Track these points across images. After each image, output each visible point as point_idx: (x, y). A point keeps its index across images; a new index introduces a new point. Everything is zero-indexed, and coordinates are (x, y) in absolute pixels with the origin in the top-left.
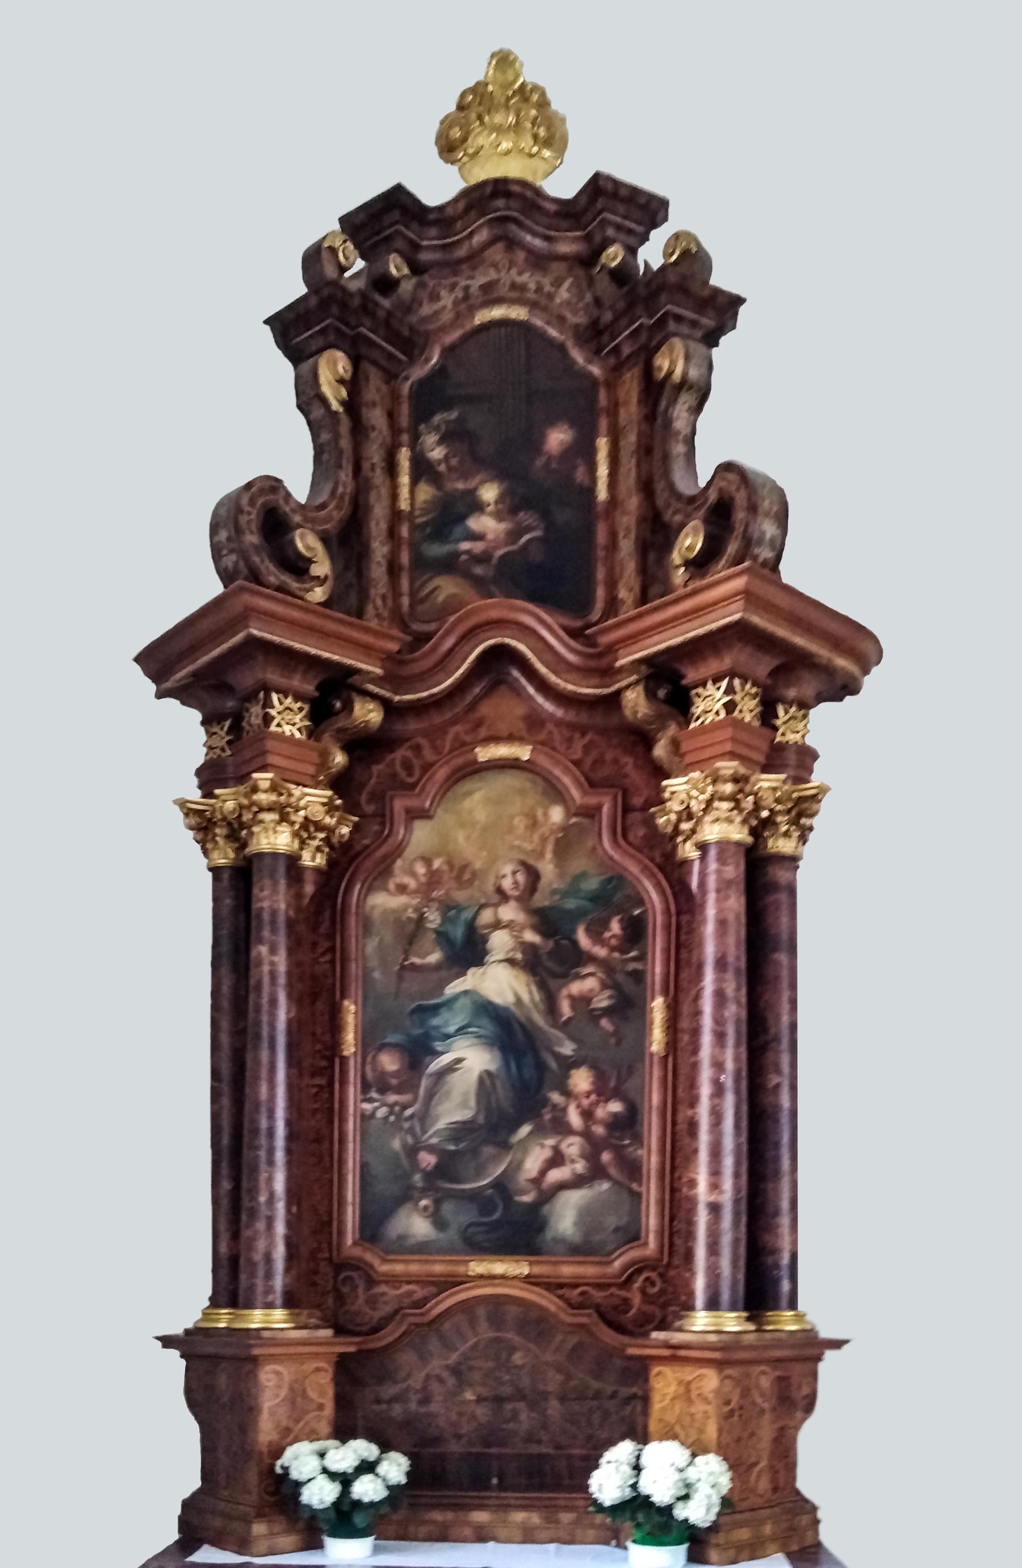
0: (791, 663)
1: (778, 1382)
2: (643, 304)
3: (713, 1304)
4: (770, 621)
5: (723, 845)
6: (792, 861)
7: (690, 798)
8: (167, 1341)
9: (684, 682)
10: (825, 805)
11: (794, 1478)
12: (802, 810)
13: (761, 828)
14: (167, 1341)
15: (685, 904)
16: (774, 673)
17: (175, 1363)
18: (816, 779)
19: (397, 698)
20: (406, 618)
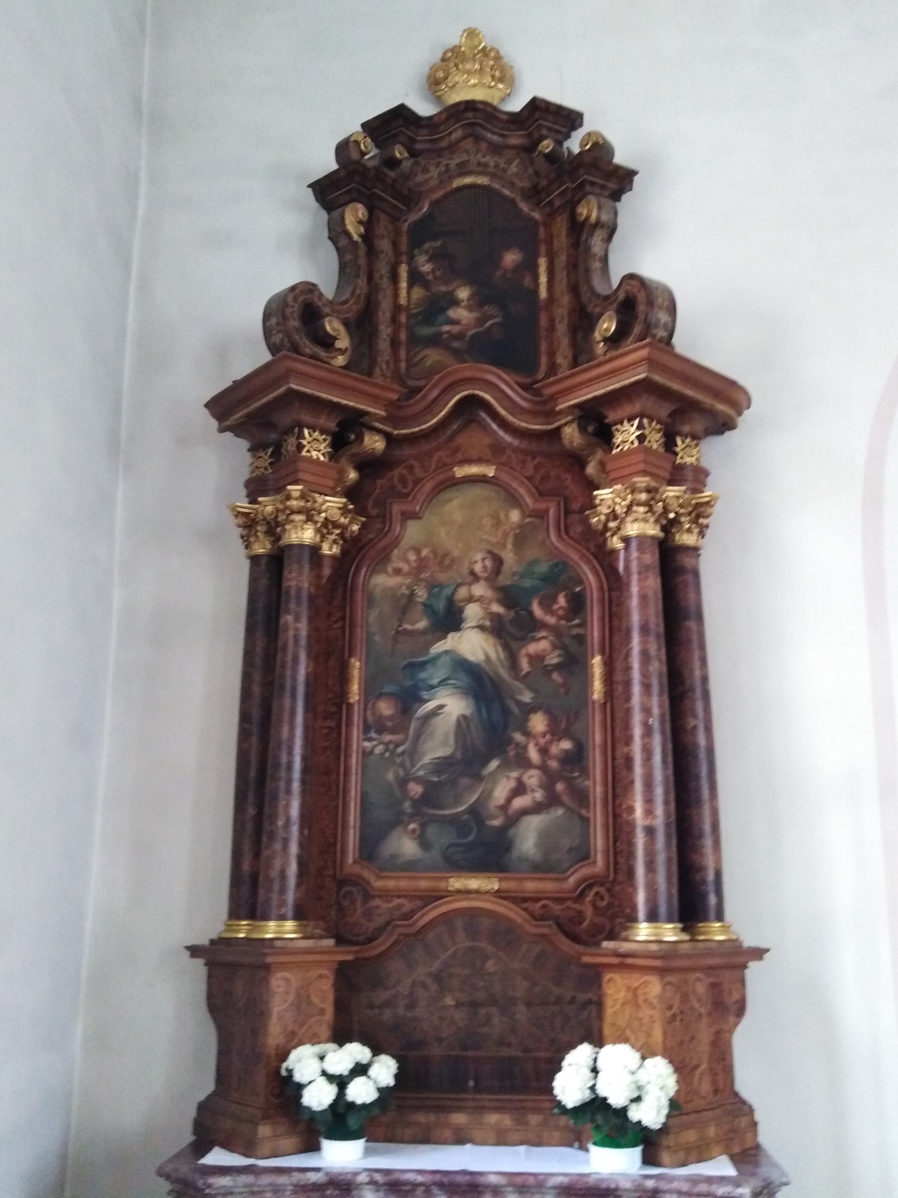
9: (607, 421)
16: (672, 414)
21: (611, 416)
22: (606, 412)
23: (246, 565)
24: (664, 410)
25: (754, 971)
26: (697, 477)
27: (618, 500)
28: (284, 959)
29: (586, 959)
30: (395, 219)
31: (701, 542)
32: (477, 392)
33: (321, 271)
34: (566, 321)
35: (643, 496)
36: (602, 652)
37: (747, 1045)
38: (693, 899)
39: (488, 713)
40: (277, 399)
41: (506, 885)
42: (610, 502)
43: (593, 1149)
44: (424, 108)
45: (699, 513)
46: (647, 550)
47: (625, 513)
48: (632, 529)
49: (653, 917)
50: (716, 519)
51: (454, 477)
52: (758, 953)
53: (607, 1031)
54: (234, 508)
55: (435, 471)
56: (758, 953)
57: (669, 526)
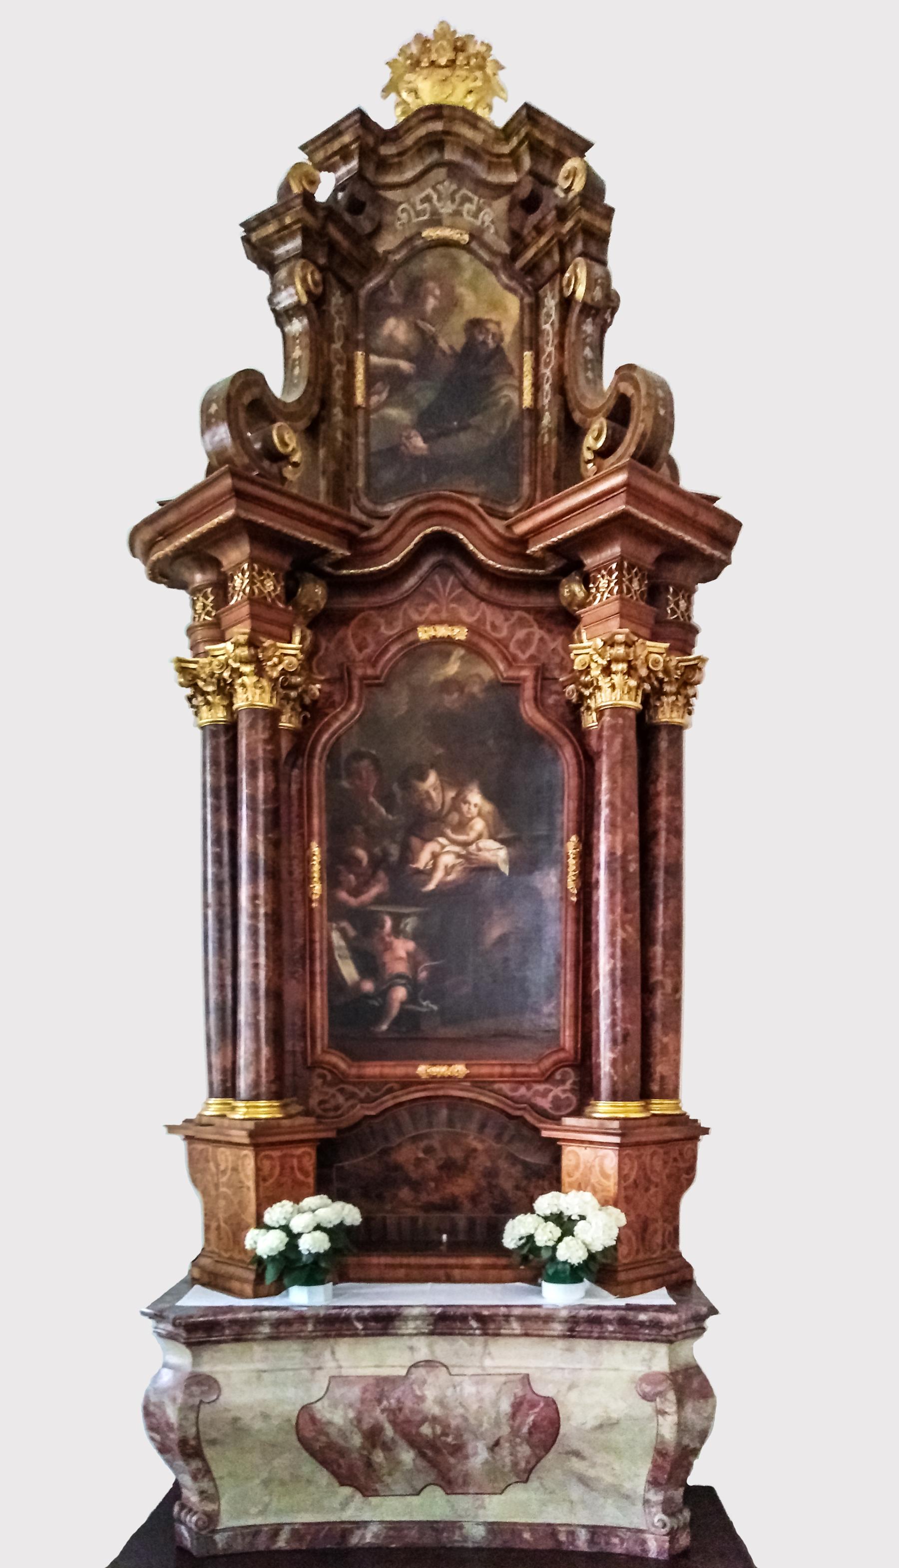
0: (675, 553)
1: (664, 1158)
2: (545, 199)
3: (614, 1096)
4: (598, 829)
5: (617, 711)
6: (676, 731)
7: (592, 660)
8: (171, 1129)
9: (585, 569)
10: (707, 669)
11: (674, 1235)
12: (688, 678)
13: (651, 699)
14: (171, 1129)
15: (588, 761)
16: (659, 560)
17: (178, 1144)
18: (697, 652)
19: (372, 799)
20: (448, 1271)
22: (582, 557)
23: (199, 732)
26: (683, 635)
29: (545, 1134)
30: (348, 289)
32: (445, 528)
33: (266, 352)
34: (550, 382)
37: (692, 1206)
39: (416, 1318)
40: (221, 526)
41: (526, 468)
43: (545, 1285)
47: (603, 663)
48: (605, 698)
51: (418, 640)
52: (706, 1131)
53: (565, 1179)
55: (417, 327)
56: (706, 1131)
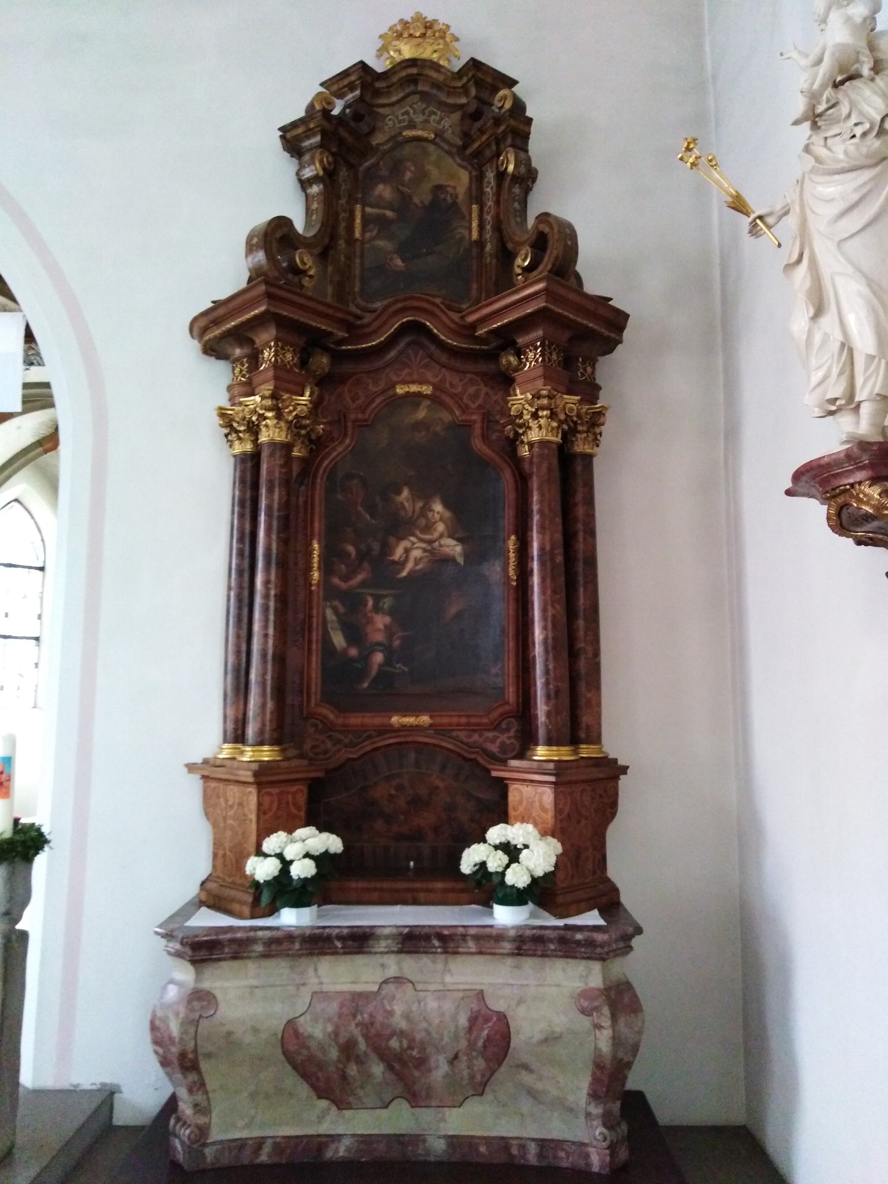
16: (570, 340)
21: (521, 341)
24: (564, 336)
25: (623, 780)
27: (527, 406)
28: (299, 776)
31: (596, 450)
35: (545, 401)
36: (516, 533)
38: (578, 717)
42: (520, 407)
44: (379, 66)
45: (595, 421)
46: (458, 236)
47: (532, 413)
49: (549, 742)
50: (608, 429)
53: (512, 813)
54: (169, 953)
57: (568, 436)
